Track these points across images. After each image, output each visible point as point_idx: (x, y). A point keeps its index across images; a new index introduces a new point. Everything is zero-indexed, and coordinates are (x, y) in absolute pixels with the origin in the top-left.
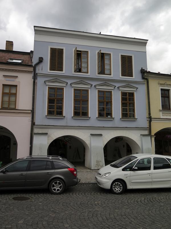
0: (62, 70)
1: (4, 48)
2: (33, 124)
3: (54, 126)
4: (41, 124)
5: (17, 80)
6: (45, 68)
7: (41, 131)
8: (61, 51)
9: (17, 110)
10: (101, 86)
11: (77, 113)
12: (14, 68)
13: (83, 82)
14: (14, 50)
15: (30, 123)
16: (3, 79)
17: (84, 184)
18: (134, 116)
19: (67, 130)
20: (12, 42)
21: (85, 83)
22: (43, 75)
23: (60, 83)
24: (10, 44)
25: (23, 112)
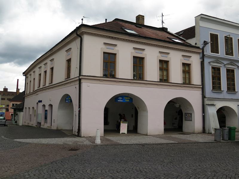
0: (219, 53)
1: (134, 21)
2: (204, 97)
3: (219, 99)
4: (211, 97)
5: (116, 48)
6: (208, 50)
7: (210, 103)
8: (216, 36)
9: (171, 83)
10: (229, 65)
11: (229, 89)
12: (112, 35)
13: (218, 62)
14: (145, 24)
15: (200, 96)
16: (104, 46)
17: (123, 145)
18: (234, 90)
19: (220, 101)
20: (144, 16)
21: (219, 62)
22: (209, 57)
23: (219, 63)
24: (140, 18)
25: (195, 87)
